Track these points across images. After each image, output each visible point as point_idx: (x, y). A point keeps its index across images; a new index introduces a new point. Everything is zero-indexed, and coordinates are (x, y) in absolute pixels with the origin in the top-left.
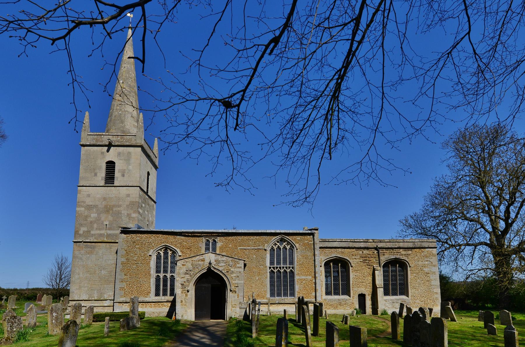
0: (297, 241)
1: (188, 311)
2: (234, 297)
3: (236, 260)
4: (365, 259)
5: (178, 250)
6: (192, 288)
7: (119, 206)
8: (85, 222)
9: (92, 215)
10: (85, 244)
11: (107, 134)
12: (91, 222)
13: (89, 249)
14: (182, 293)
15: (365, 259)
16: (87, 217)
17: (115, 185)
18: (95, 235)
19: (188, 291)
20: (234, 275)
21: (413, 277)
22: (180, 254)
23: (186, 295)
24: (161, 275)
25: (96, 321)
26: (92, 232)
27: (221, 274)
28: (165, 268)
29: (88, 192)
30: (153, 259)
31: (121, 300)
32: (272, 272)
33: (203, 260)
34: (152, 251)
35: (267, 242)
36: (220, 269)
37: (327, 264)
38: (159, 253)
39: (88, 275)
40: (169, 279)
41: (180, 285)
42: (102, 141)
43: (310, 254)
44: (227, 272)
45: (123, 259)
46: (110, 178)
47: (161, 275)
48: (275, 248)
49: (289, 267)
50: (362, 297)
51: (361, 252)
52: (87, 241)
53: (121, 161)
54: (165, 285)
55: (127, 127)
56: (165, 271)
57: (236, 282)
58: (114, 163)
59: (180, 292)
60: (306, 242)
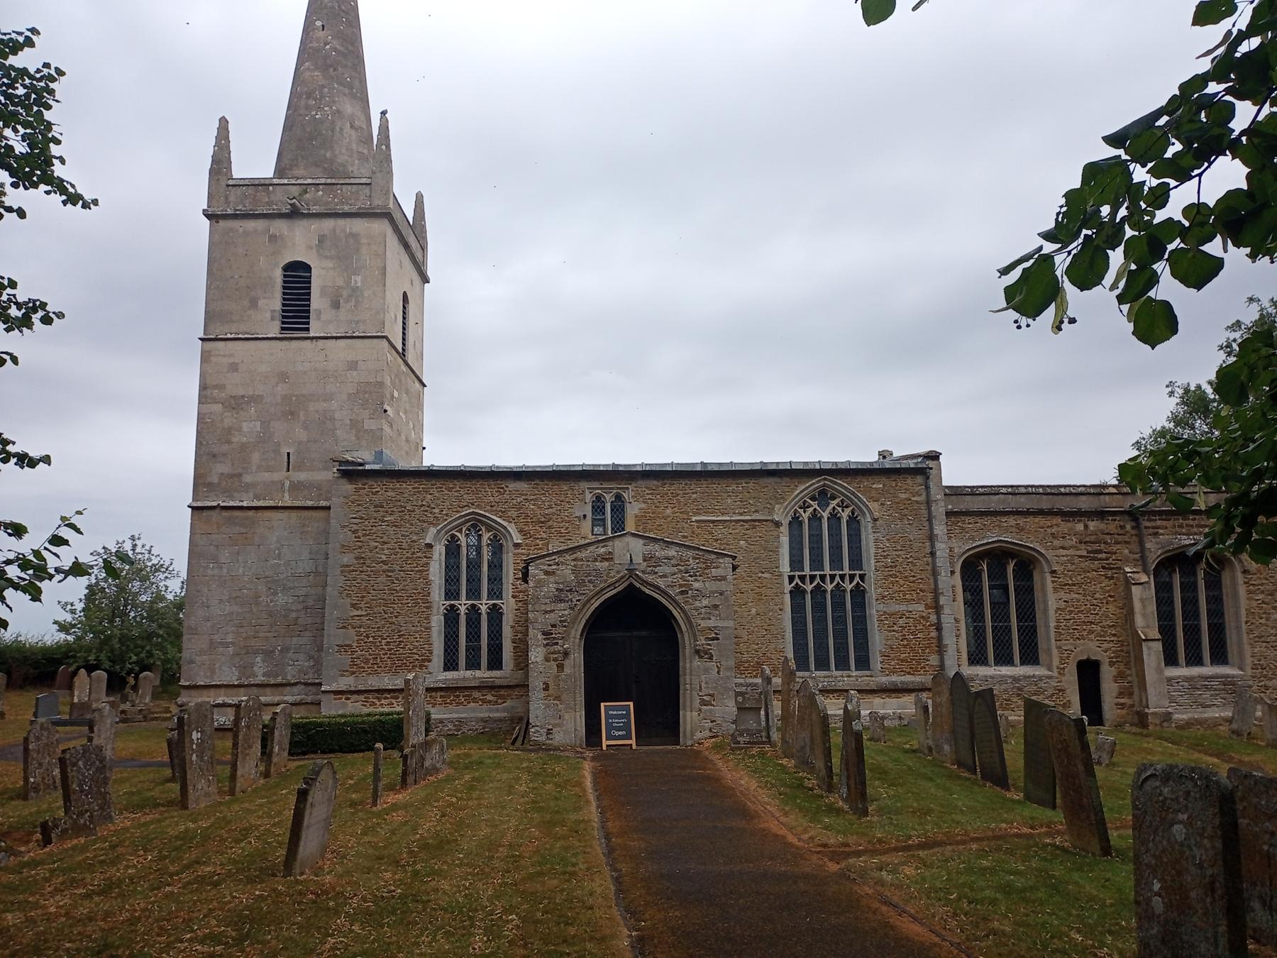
0: (874, 494)
1: (567, 716)
2: (707, 671)
3: (707, 556)
4: (1096, 547)
5: (512, 529)
6: (574, 643)
7: (328, 398)
8: (225, 448)
9: (245, 427)
10: (225, 514)
11: (286, 181)
12: (243, 447)
13: (237, 529)
14: (547, 660)
15: (1096, 547)
16: (229, 431)
17: (312, 334)
18: (254, 485)
19: (566, 654)
20: (705, 602)
21: (1254, 604)
22: (518, 539)
23: (561, 667)
24: (463, 605)
25: (169, 746)
26: (247, 479)
27: (664, 601)
28: (474, 582)
29: (231, 355)
30: (436, 556)
31: (345, 683)
32: (797, 593)
33: (608, 558)
34: (433, 530)
35: (780, 499)
36: (661, 583)
37: (970, 569)
38: (453, 536)
39: (235, 608)
40: (484, 618)
41: (540, 636)
42: (270, 203)
43: (915, 534)
44: (682, 593)
45: (347, 559)
46: (296, 314)
47: (463, 605)
48: (805, 516)
49: (813, 578)
50: (1088, 672)
51: (1080, 527)
52: (232, 504)
53: (330, 264)
54: (474, 635)
55: (341, 159)
56: (474, 593)
57: (711, 623)
58: (308, 268)
59: (540, 659)
60: (903, 496)
